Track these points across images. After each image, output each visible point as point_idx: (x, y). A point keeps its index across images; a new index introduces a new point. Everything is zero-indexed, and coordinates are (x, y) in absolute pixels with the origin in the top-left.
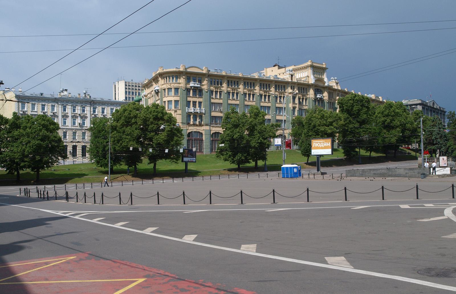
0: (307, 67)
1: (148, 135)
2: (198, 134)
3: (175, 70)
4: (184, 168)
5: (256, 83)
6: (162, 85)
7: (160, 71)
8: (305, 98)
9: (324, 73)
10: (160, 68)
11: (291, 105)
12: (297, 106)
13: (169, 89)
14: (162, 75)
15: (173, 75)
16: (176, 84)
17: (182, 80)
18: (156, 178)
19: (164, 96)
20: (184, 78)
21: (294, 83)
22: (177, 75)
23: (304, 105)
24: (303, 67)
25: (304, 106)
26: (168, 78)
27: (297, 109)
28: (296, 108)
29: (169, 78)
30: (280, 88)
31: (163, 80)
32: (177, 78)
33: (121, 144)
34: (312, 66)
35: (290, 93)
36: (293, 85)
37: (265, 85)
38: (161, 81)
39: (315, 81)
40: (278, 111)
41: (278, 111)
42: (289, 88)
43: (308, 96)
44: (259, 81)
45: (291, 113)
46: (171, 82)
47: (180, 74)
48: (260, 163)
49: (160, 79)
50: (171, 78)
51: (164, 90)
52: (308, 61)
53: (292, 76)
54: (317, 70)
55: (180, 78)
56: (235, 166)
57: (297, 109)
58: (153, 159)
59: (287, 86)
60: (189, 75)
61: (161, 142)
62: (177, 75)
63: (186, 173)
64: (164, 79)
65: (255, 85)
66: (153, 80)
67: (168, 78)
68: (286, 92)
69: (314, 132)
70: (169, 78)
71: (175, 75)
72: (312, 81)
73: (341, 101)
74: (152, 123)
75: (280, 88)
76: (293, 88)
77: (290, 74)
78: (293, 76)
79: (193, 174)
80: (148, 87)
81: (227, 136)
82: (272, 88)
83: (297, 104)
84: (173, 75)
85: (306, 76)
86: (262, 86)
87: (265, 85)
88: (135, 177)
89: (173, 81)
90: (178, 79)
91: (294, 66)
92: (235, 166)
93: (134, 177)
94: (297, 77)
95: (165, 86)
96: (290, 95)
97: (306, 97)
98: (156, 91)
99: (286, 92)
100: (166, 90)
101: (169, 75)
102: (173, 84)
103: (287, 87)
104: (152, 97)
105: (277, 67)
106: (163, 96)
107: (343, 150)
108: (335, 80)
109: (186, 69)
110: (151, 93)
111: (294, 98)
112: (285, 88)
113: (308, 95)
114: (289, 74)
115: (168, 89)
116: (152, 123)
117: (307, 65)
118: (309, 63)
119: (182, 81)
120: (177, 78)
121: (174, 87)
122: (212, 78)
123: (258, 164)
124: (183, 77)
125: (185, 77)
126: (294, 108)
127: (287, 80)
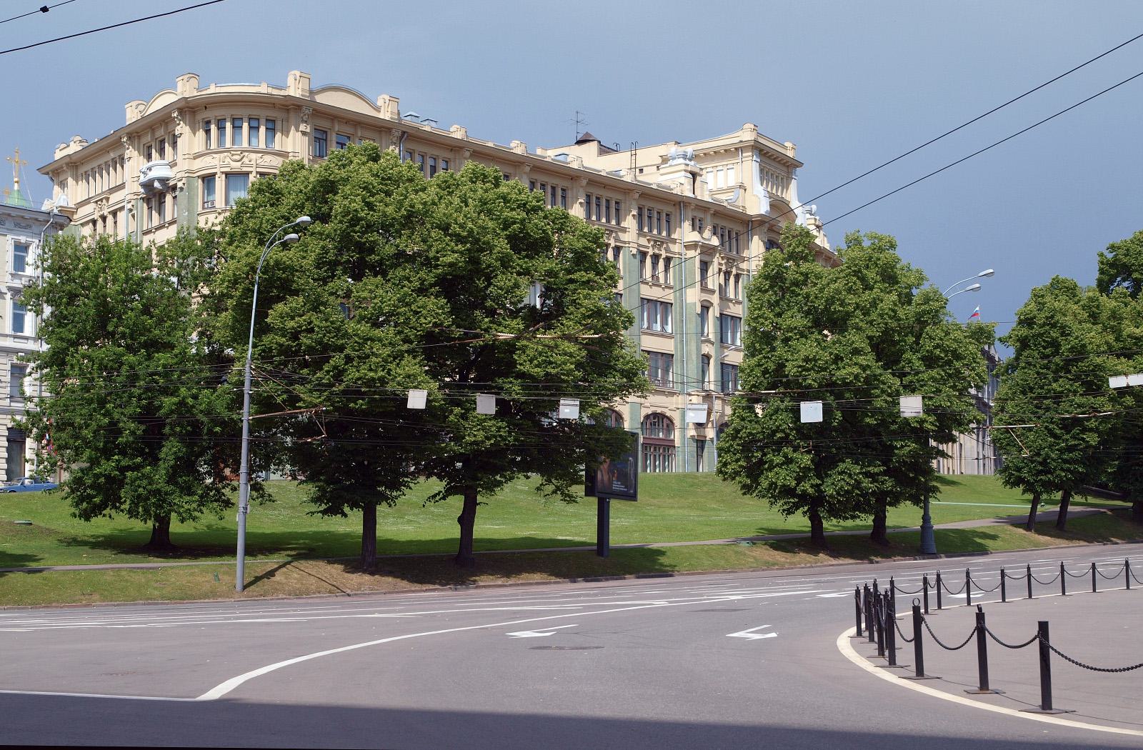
0: (736, 149)
1: (486, 330)
2: (660, 363)
3: (263, 89)
4: (588, 534)
5: (572, 189)
6: (195, 158)
7: (186, 89)
8: (734, 271)
9: (789, 179)
10: (186, 77)
11: (693, 296)
12: (715, 299)
13: (232, 179)
14: (192, 111)
15: (255, 112)
16: (268, 158)
17: (294, 138)
18: (525, 575)
19: (203, 208)
20: (304, 133)
21: (702, 207)
22: (272, 114)
23: (731, 301)
24: (716, 150)
25: (731, 305)
26: (228, 125)
27: (714, 313)
28: (711, 310)
29: (221, 129)
30: (655, 220)
31: (201, 134)
32: (271, 131)
33: (339, 374)
34: (759, 149)
35: (692, 246)
36: (700, 215)
37: (604, 203)
38: (189, 139)
39: (769, 209)
40: (645, 314)
41: (645, 314)
42: (687, 225)
43: (744, 266)
44: (584, 182)
45: (692, 326)
46: (245, 144)
47: (288, 111)
48: (903, 517)
49: (182, 129)
50: (245, 126)
51: (208, 180)
52: (739, 127)
53: (694, 175)
54: (776, 166)
55: (286, 133)
56: (799, 522)
57: (714, 313)
58: (473, 475)
59: (678, 214)
60: (324, 124)
61: (569, 373)
62: (272, 114)
63: (598, 562)
64: (208, 132)
65: (569, 200)
66: (129, 138)
67: (228, 125)
68: (674, 241)
69: (1074, 380)
70: (221, 129)
71: (263, 113)
72: (756, 203)
73: (1126, 255)
74: (505, 263)
75: (655, 220)
76: (698, 226)
77: (689, 169)
78: (698, 178)
79: (644, 563)
80: (79, 173)
81: (808, 370)
82: (630, 218)
83: (713, 292)
84: (255, 112)
85: (738, 185)
86: (594, 206)
87: (604, 203)
88: (372, 574)
89: (254, 140)
90: (278, 135)
91: (677, 143)
92: (799, 522)
93: (364, 572)
94: (711, 186)
95: (216, 162)
96: (691, 253)
97: (738, 268)
98: (157, 184)
99: (674, 241)
100: (220, 183)
101: (238, 112)
102: (253, 156)
103: (678, 220)
104: (110, 219)
105: (593, 147)
106: (200, 209)
107: (378, 508)
108: (811, 214)
109: (312, 92)
110: (107, 199)
111: (705, 266)
112: (670, 223)
113: (743, 260)
114: (683, 167)
115: (227, 175)
116: (505, 263)
117: (736, 140)
118: (747, 135)
119: (296, 144)
120: (271, 131)
121: (259, 170)
122: (412, 146)
123: (379, 533)
124: (302, 127)
125: (308, 130)
126: (706, 307)
127: (677, 191)
